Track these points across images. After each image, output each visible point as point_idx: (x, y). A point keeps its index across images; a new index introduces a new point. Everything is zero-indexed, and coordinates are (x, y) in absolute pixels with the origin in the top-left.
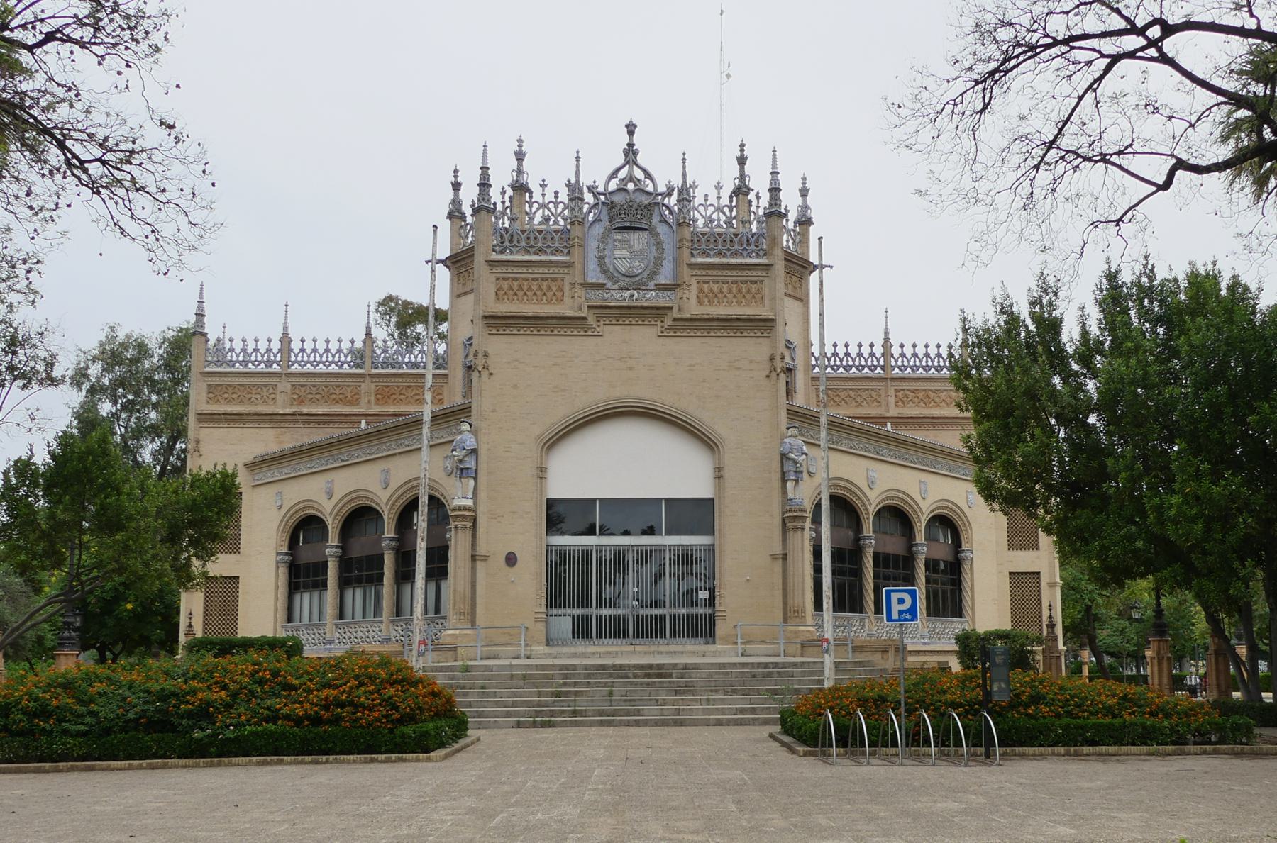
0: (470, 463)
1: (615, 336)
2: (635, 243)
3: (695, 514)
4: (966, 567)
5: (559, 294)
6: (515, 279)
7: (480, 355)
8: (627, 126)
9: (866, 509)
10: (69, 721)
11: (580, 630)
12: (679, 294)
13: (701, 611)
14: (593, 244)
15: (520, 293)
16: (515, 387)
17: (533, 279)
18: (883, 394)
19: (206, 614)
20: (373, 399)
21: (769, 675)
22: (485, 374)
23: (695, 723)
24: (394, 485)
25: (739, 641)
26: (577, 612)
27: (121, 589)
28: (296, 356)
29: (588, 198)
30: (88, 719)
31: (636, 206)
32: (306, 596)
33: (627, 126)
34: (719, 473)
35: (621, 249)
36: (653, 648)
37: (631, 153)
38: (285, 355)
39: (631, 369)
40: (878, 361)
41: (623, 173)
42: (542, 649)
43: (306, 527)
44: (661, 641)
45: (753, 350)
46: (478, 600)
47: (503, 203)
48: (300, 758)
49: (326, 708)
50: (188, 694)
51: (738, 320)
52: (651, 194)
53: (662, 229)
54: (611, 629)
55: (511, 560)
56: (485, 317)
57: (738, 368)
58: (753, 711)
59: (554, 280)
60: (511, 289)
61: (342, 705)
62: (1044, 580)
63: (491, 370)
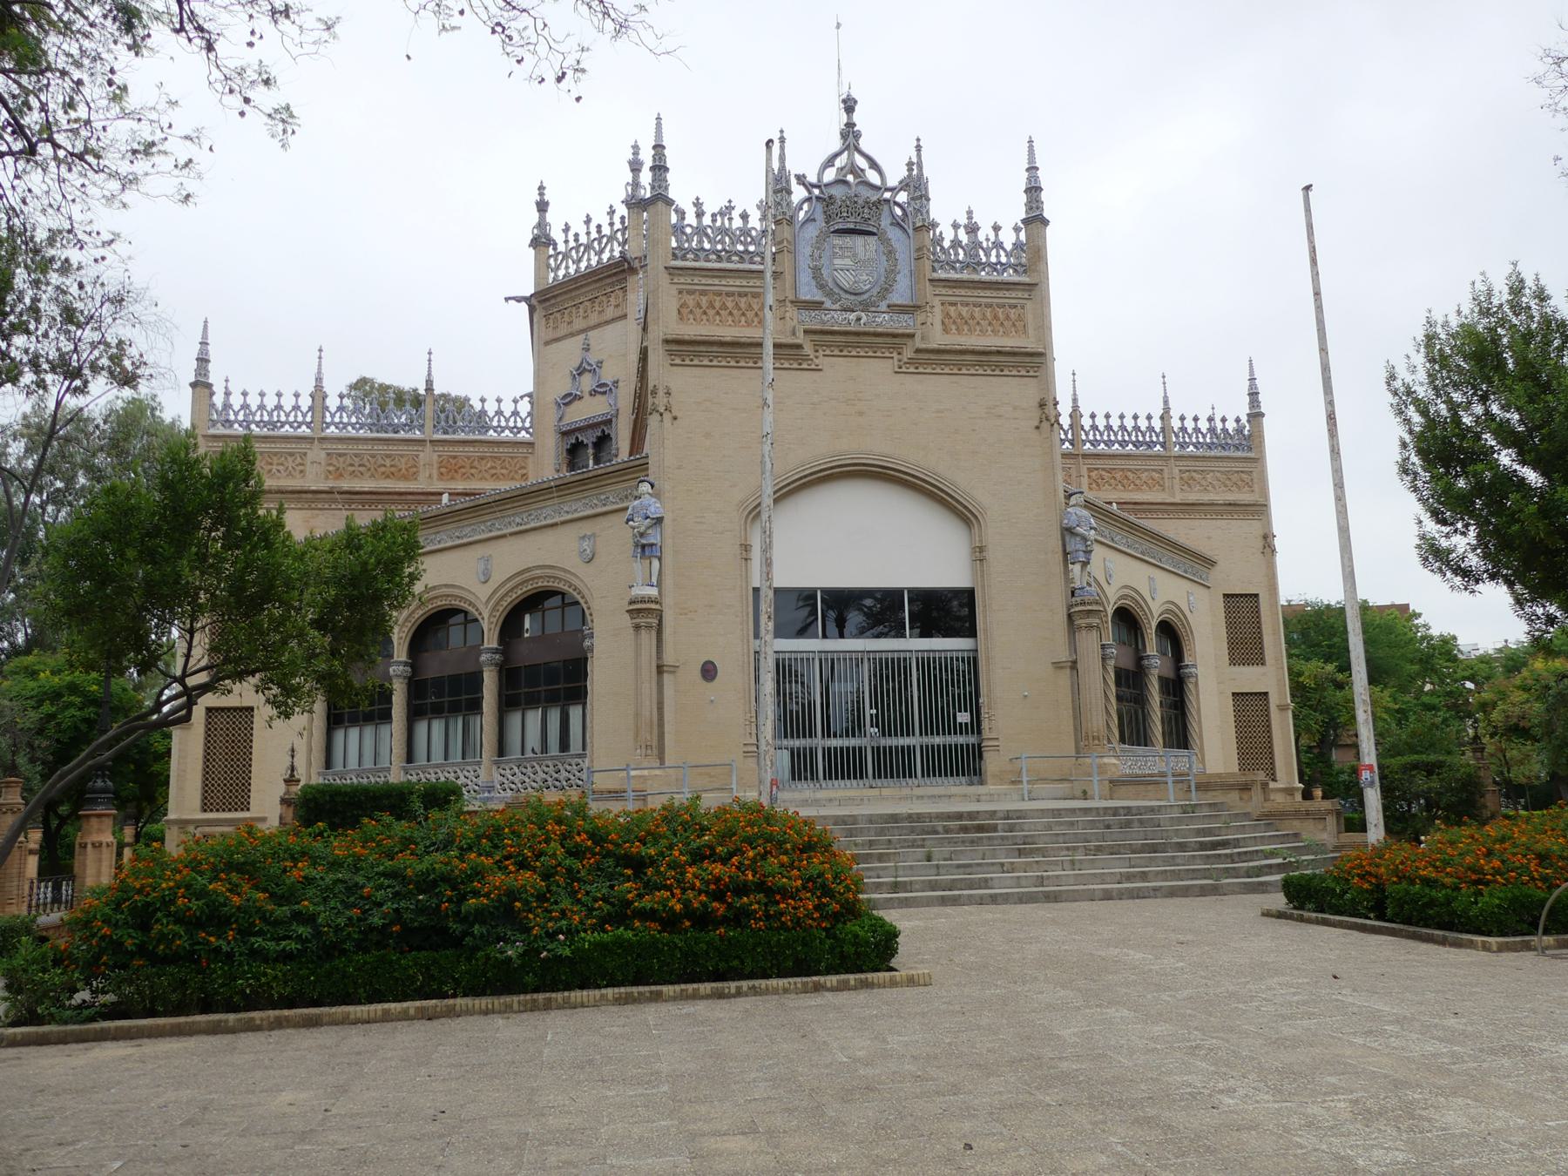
0: (653, 537)
1: (837, 371)
2: (860, 250)
3: (945, 611)
6: (703, 293)
8: (844, 101)
10: (260, 933)
12: (920, 317)
13: (961, 740)
14: (805, 250)
15: (711, 312)
17: (728, 294)
18: (1074, 474)
19: (206, 760)
20: (435, 473)
21: (1128, 824)
23: (1074, 897)
24: (498, 577)
25: (1025, 779)
26: (797, 743)
27: (83, 727)
28: (333, 416)
29: (799, 193)
30: (303, 930)
31: (860, 202)
32: (354, 733)
33: (844, 101)
34: (979, 554)
35: (842, 257)
36: (906, 791)
37: (850, 134)
38: (318, 415)
39: (861, 414)
40: (523, 421)
41: (841, 161)
44: (910, 781)
45: (1013, 391)
46: (667, 728)
47: (612, 224)
48: (690, 987)
49: (719, 896)
50: (470, 878)
51: (999, 352)
52: (877, 188)
53: (894, 234)
55: (709, 671)
56: (667, 342)
58: (1144, 876)
60: (699, 306)
61: (742, 890)
62: (1274, 701)
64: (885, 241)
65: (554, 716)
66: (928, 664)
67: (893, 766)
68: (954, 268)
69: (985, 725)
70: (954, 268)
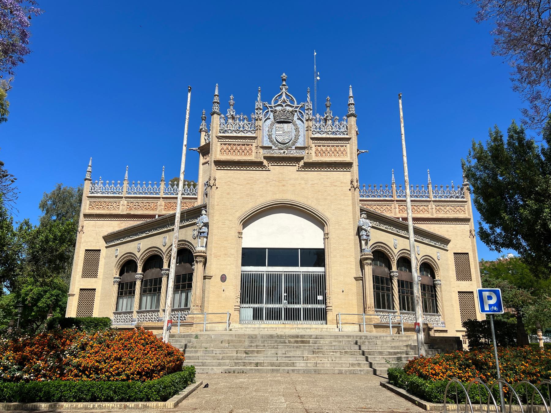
3: (317, 257)
4: (438, 289)
5: (250, 151)
7: (212, 179)
9: (393, 258)
11: (257, 315)
13: (319, 306)
15: (232, 151)
16: (228, 194)
22: (214, 188)
26: (256, 306)
34: (326, 237)
35: (279, 131)
36: (295, 326)
39: (284, 186)
42: (237, 325)
43: (128, 266)
44: (298, 322)
54: (274, 315)
55: (223, 278)
57: (335, 186)
59: (248, 145)
63: (217, 186)
64: (295, 125)
65: (184, 295)
66: (307, 277)
67: (292, 315)
68: (328, 134)
69: (328, 301)
70: (328, 134)
